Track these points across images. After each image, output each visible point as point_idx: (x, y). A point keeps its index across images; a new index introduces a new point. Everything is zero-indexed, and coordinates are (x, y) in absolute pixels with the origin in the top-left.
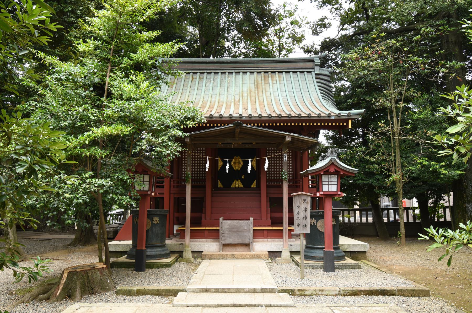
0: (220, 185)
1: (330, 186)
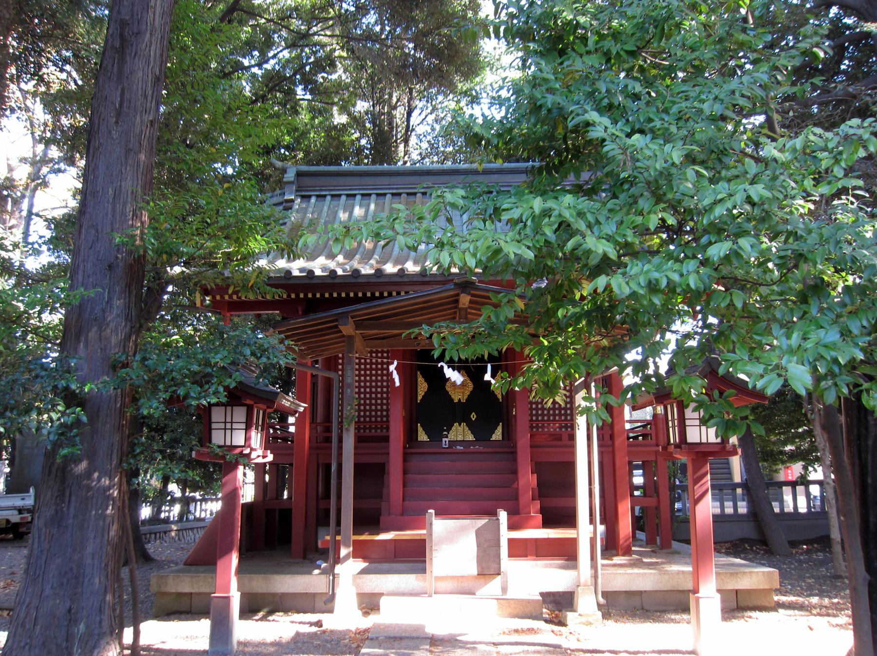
0: (423, 436)
1: (229, 432)
